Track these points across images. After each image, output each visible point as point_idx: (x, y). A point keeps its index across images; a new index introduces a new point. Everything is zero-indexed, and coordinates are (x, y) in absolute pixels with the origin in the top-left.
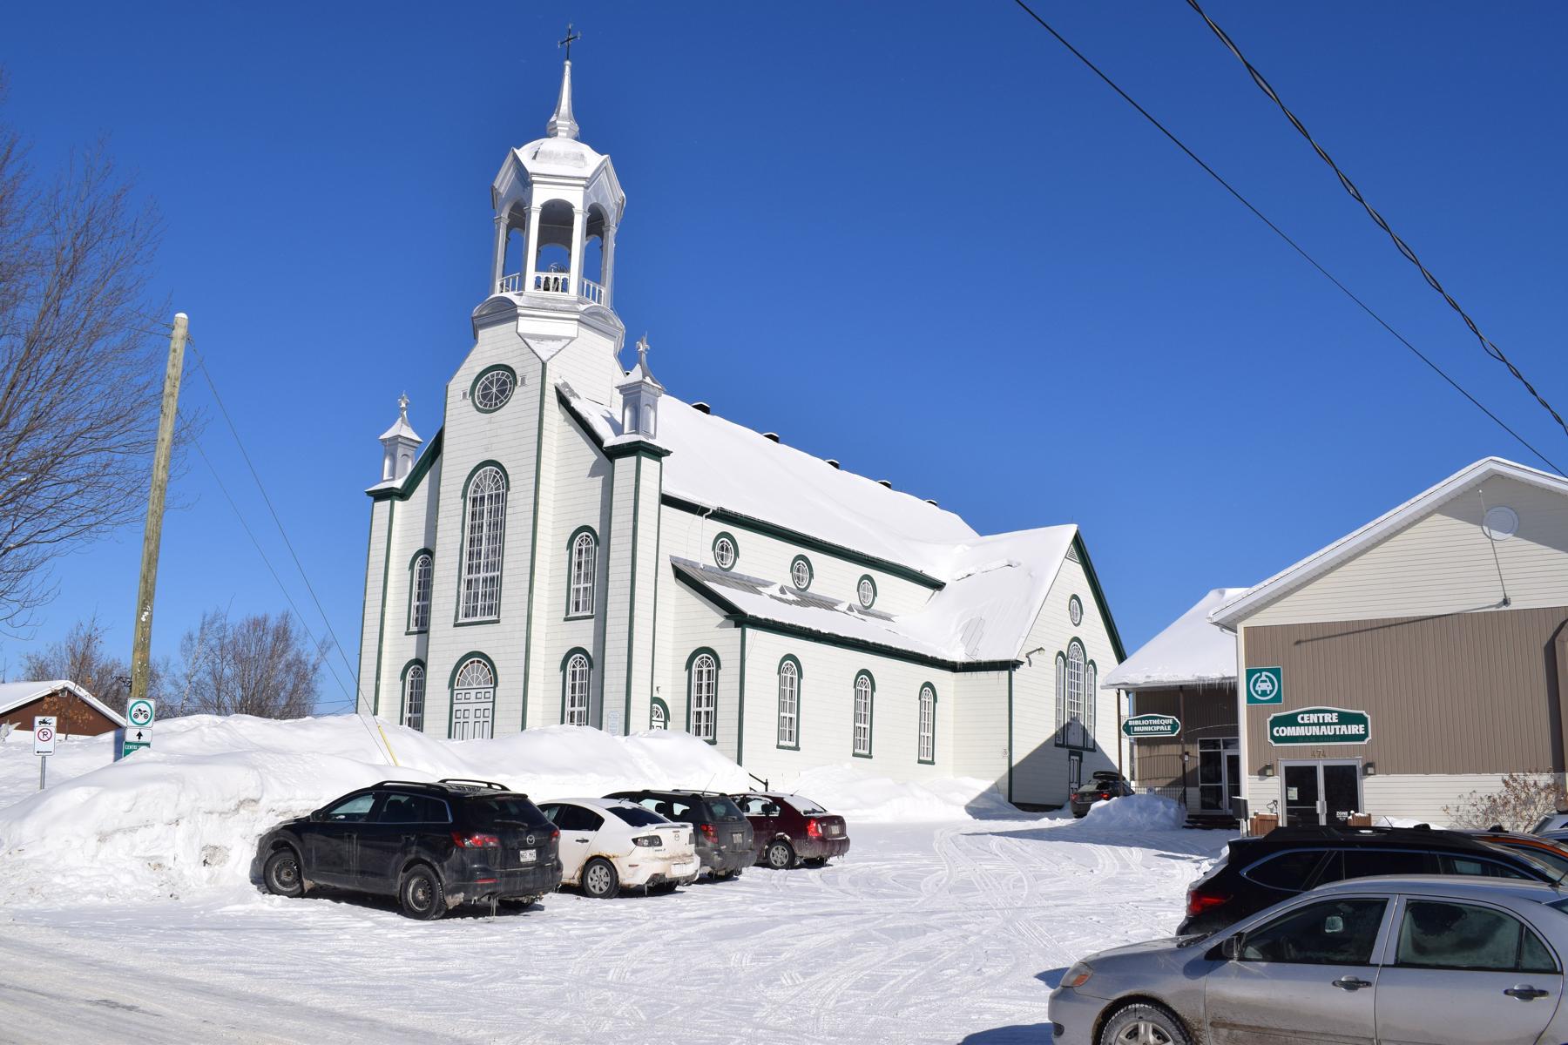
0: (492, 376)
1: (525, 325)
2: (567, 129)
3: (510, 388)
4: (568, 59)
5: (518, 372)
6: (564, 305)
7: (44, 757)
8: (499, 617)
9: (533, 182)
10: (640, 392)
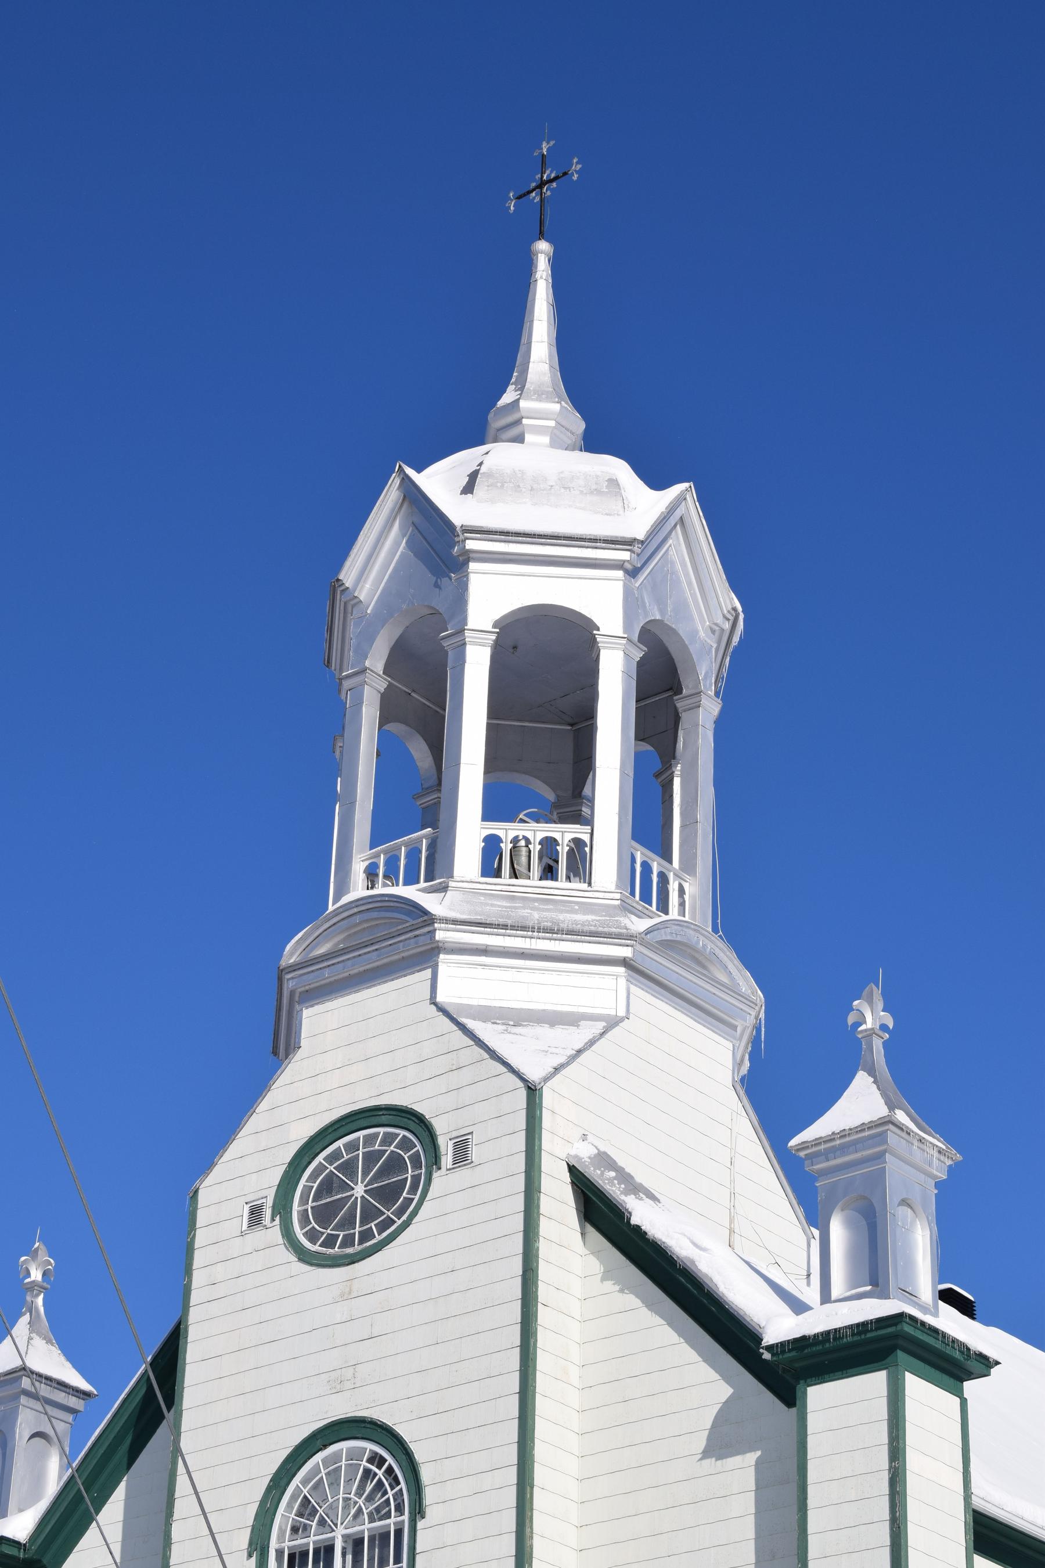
0: (352, 1147)
2: (552, 423)
3: (416, 1180)
4: (541, 235)
6: (580, 917)
9: (468, 557)
10: (880, 1157)
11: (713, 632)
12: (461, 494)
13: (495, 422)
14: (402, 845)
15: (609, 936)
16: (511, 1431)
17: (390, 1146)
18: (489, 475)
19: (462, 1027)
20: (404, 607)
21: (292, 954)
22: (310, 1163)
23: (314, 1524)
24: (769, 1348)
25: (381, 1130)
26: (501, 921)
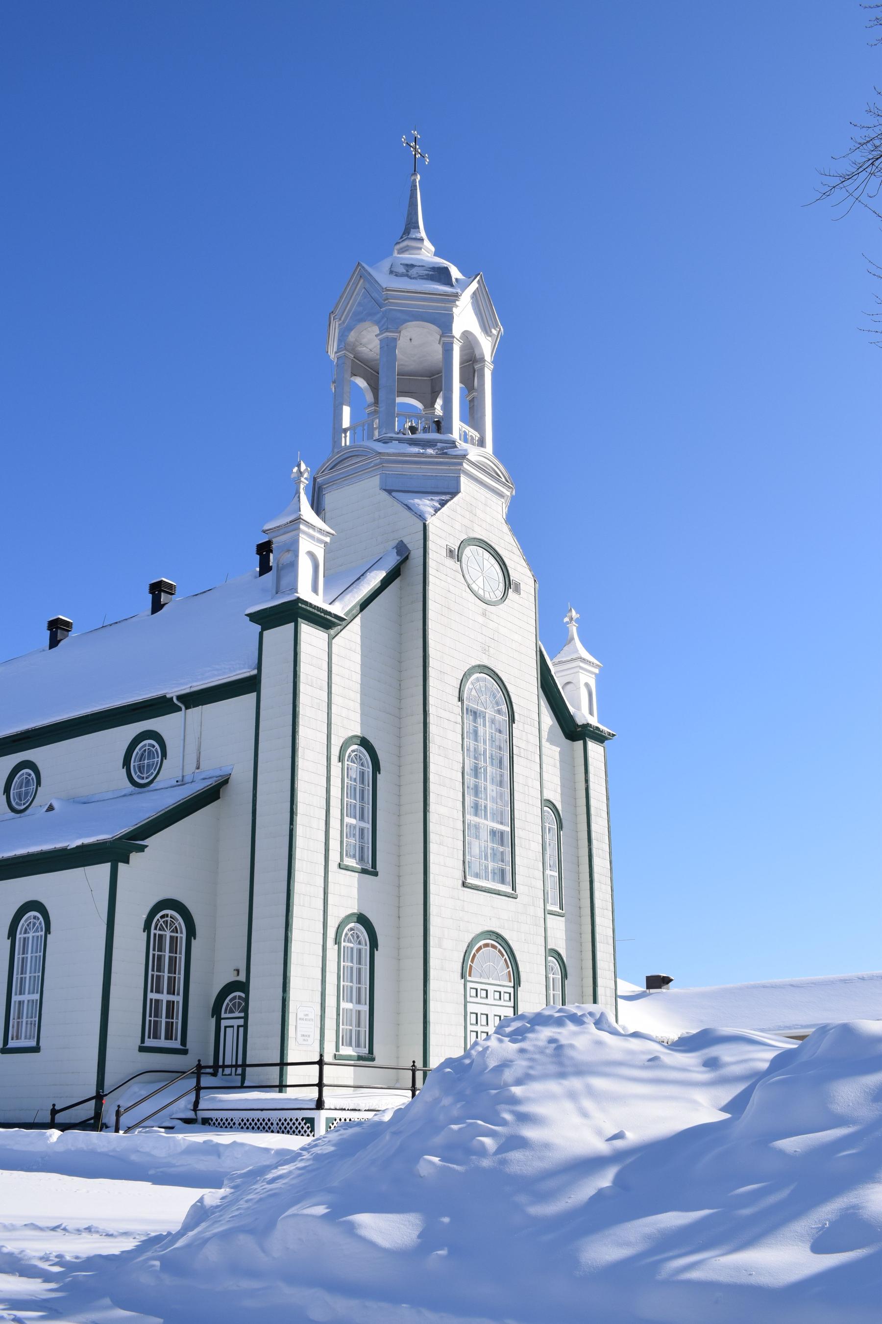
8: (184, 1042)
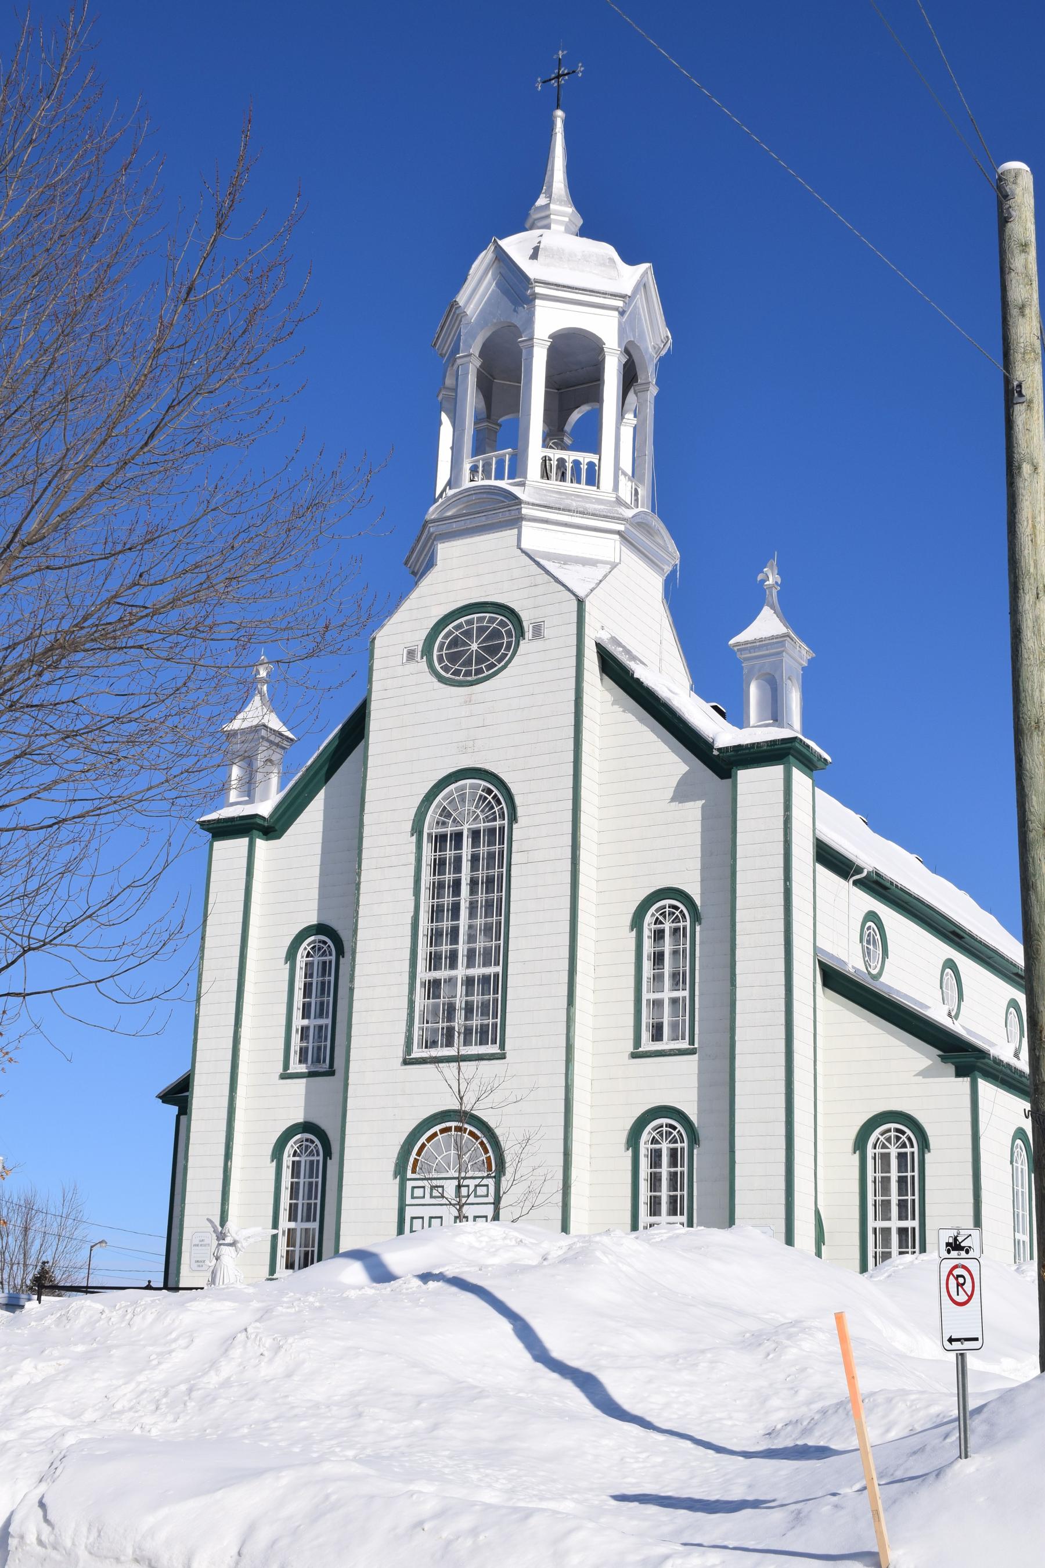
0: (470, 622)
1: (533, 536)
5: (524, 616)
7: (961, 1357)
8: (502, 1046)
9: (535, 296)
10: (780, 653)
11: (655, 348)
12: (530, 259)
13: (534, 215)
14: (493, 456)
15: (613, 518)
16: (569, 782)
17: (493, 624)
18: (545, 249)
19: (538, 564)
20: (495, 321)
21: (433, 513)
22: (443, 629)
23: (450, 821)
24: (719, 750)
25: (488, 615)
26: (557, 506)
